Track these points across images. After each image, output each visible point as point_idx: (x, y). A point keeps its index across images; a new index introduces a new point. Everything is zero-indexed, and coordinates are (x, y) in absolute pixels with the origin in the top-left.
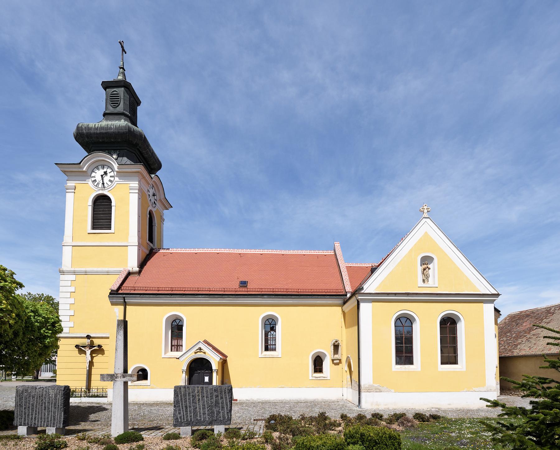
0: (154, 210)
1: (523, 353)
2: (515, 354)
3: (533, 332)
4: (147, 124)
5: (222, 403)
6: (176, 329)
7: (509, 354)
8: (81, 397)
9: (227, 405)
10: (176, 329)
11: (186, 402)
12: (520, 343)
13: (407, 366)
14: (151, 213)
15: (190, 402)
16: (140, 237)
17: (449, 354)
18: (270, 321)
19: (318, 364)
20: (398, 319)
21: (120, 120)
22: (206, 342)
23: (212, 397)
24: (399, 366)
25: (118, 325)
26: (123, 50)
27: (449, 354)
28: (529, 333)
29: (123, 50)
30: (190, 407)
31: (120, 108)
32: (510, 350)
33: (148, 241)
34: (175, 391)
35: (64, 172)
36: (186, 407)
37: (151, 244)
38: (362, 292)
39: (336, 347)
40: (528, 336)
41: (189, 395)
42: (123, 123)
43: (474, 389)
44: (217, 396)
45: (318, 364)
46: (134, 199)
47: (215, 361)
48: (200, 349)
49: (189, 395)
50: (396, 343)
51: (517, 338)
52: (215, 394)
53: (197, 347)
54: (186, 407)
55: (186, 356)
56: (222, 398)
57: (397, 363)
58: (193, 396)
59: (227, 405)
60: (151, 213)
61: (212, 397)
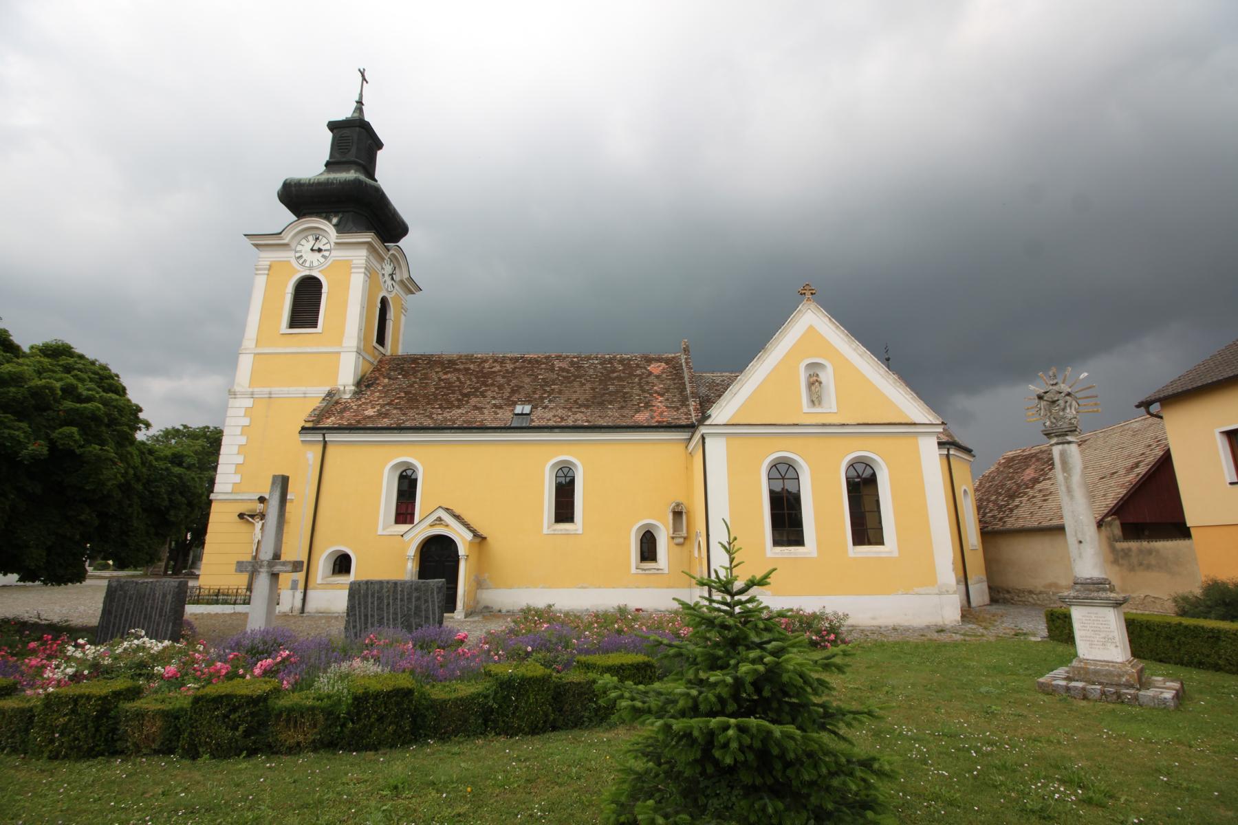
0: (388, 296)
1: (1020, 524)
2: (1008, 526)
3: (1038, 486)
4: (391, 174)
5: (427, 610)
6: (407, 487)
7: (999, 526)
8: (235, 603)
9: (434, 613)
10: (407, 487)
11: (366, 608)
12: (1017, 506)
13: (793, 549)
14: (384, 302)
15: (372, 609)
16: (364, 338)
17: (866, 527)
18: (566, 470)
19: (648, 548)
20: (775, 466)
21: (348, 170)
22: (447, 510)
23: (409, 599)
24: (778, 549)
25: (274, 483)
26: (364, 79)
27: (866, 527)
28: (1032, 488)
29: (364, 79)
30: (372, 616)
31: (352, 156)
32: (1001, 519)
33: (375, 343)
34: (351, 589)
35: (256, 246)
36: (366, 616)
37: (380, 348)
38: (708, 422)
39: (677, 514)
40: (1031, 493)
41: (373, 596)
42: (351, 175)
43: (916, 590)
44: (418, 599)
45: (648, 548)
46: (357, 281)
47: (462, 538)
48: (440, 519)
49: (373, 596)
50: (772, 509)
51: (1012, 497)
52: (415, 594)
53: (434, 516)
54: (366, 616)
55: (420, 531)
56: (426, 601)
57: (776, 543)
58: (379, 598)
59: (434, 613)
60: (384, 302)
61: (409, 599)
